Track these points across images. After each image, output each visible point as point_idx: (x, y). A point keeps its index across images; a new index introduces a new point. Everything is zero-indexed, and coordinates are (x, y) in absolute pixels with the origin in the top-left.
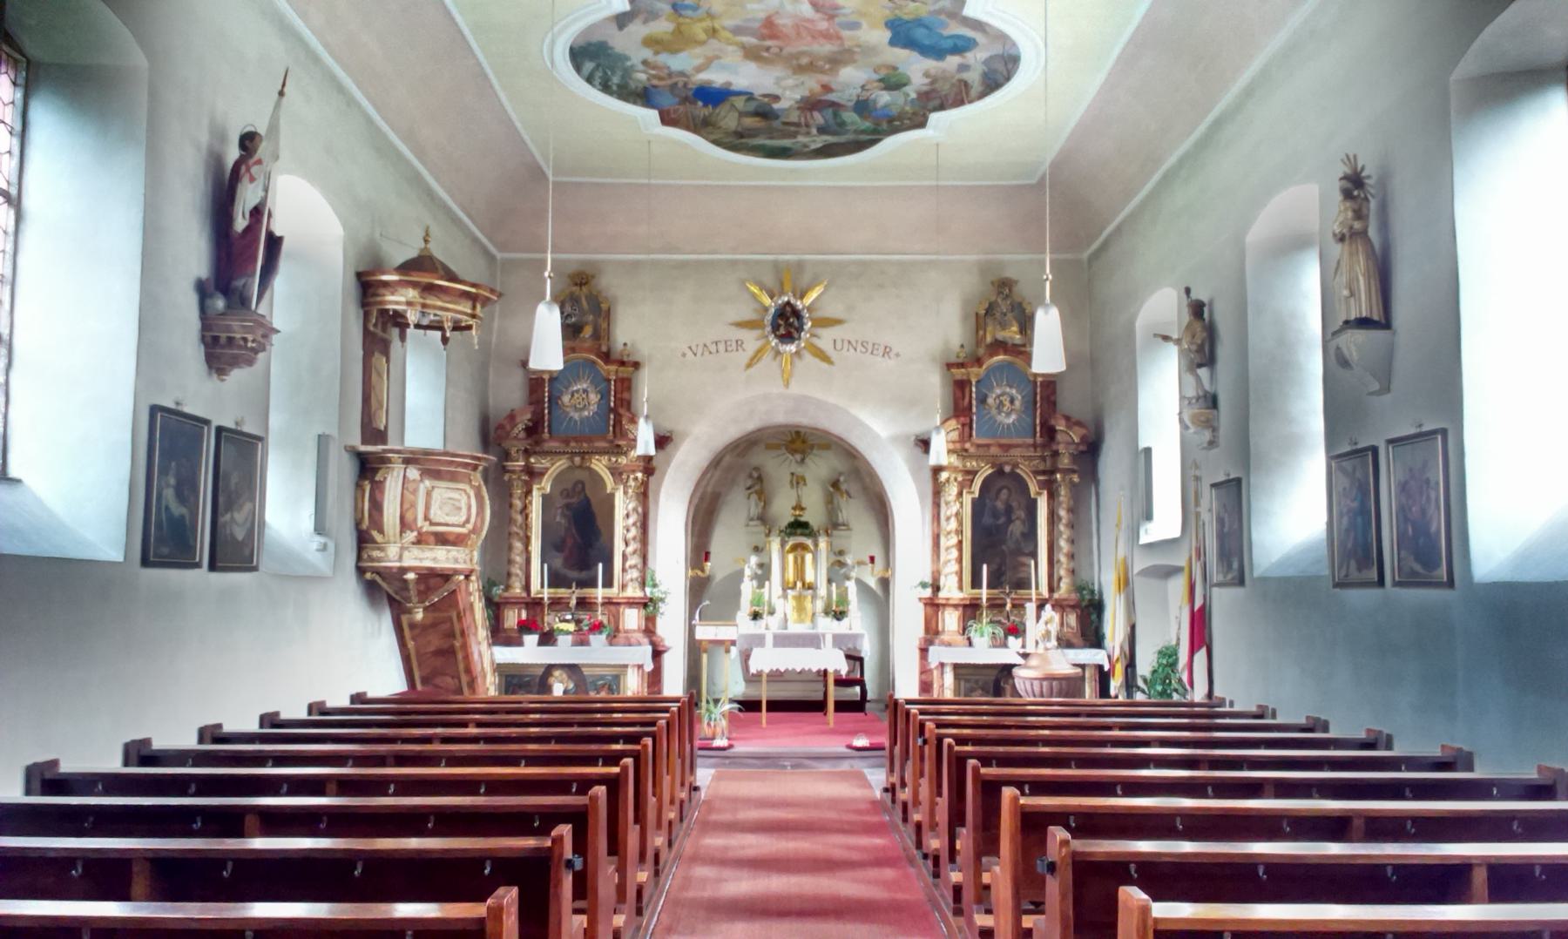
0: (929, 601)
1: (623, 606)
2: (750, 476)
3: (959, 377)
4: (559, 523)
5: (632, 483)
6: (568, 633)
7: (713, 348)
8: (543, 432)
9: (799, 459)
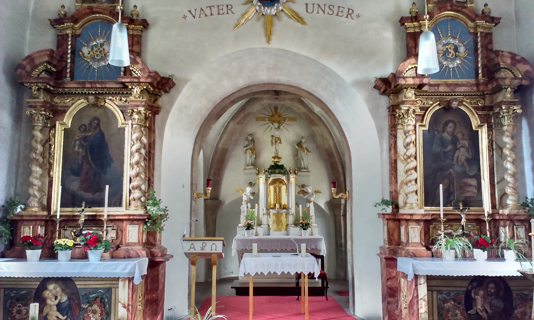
0: (391, 217)
1: (125, 223)
2: (247, 139)
3: (411, 31)
4: (78, 153)
5: (136, 116)
6: (67, 247)
7: (208, 12)
8: (66, 77)
9: (276, 127)
